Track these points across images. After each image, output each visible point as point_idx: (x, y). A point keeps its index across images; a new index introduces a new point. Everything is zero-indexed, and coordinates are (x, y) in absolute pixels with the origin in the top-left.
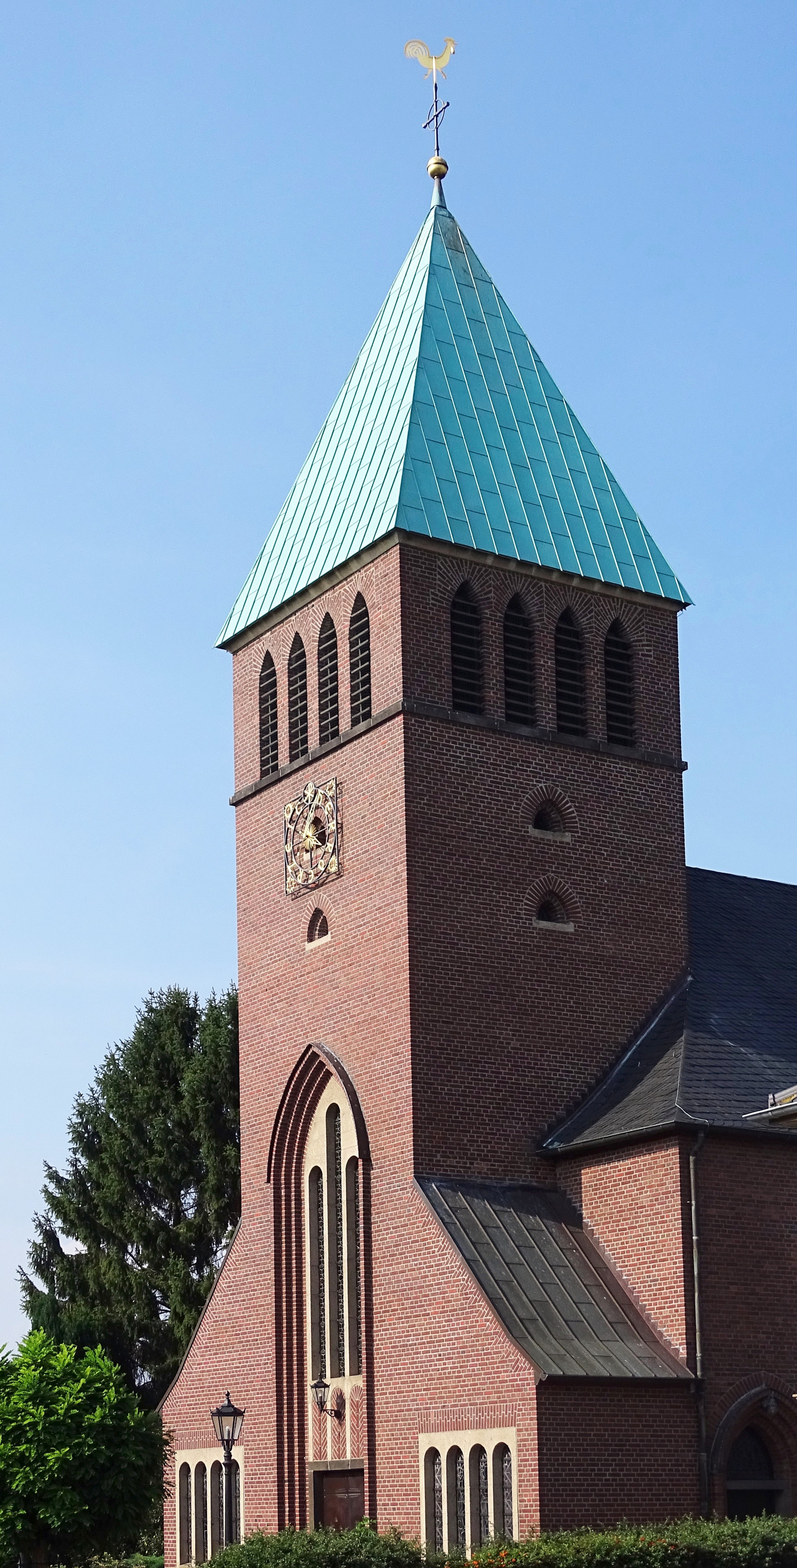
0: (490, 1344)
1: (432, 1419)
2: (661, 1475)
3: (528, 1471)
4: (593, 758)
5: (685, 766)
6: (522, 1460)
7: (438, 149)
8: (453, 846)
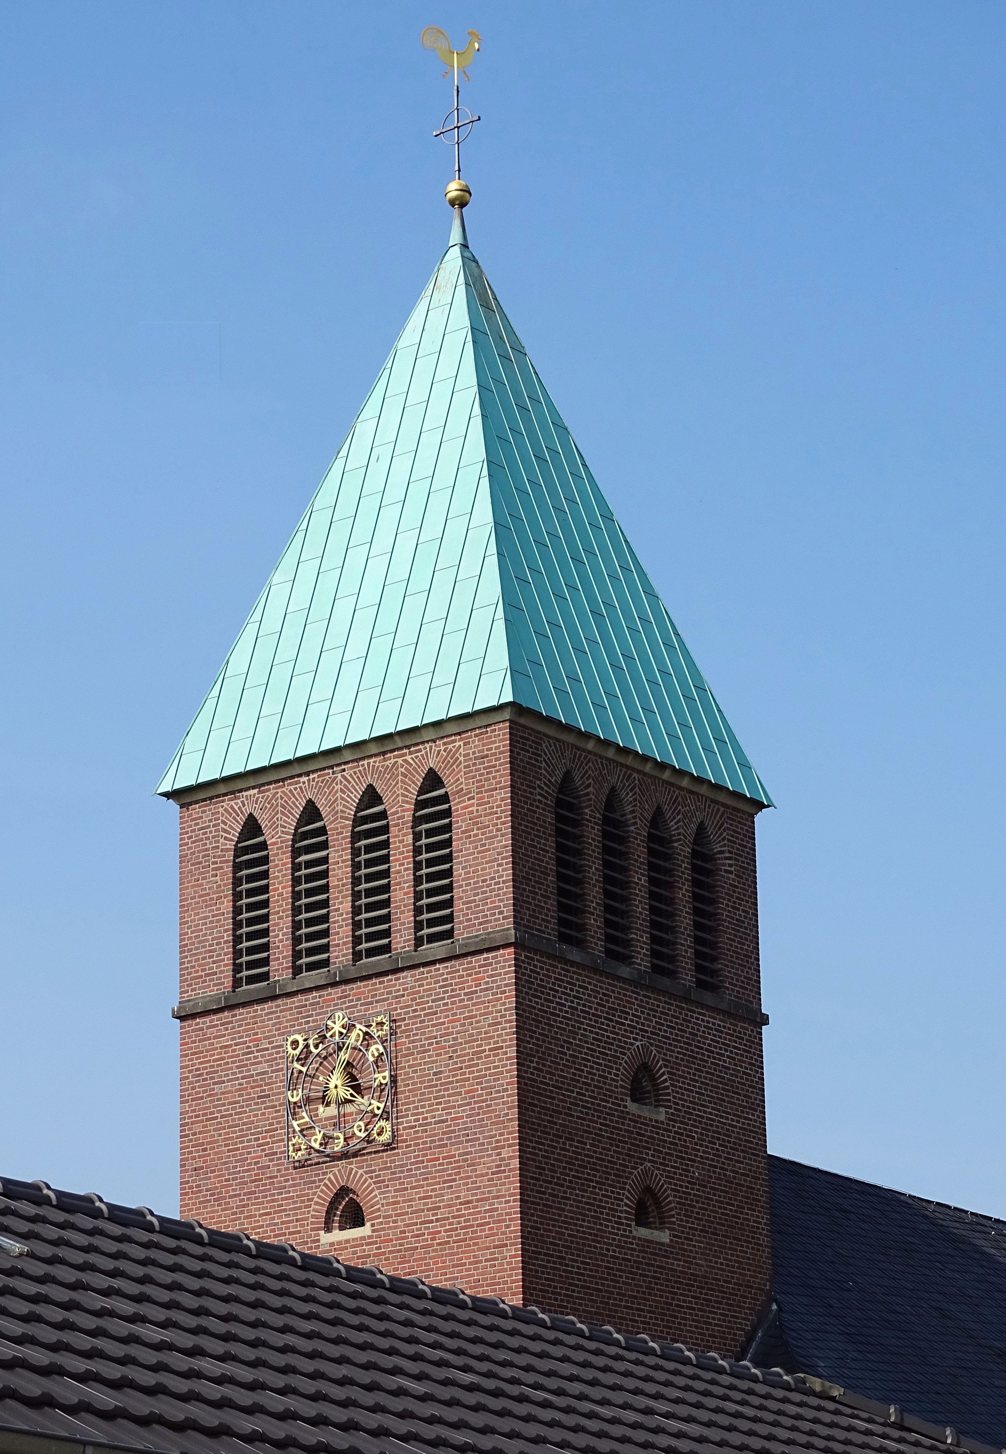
5: (765, 1020)
7: (459, 170)
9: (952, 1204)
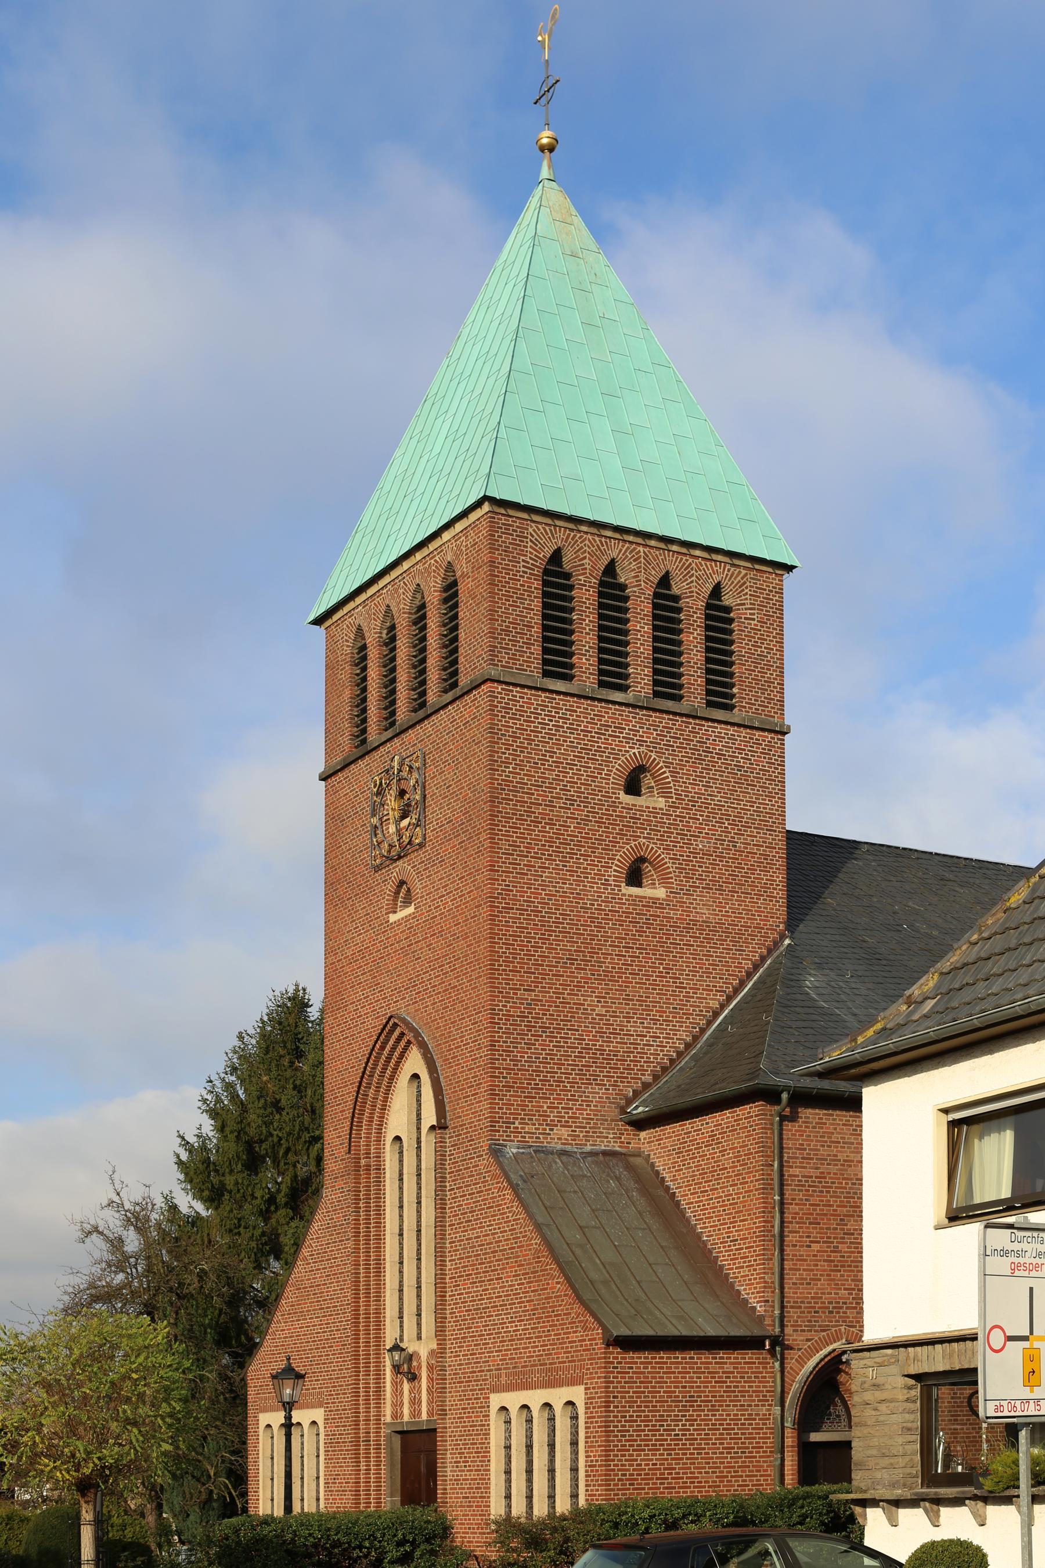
0: (560, 1306)
1: (503, 1380)
2: (733, 1429)
3: (594, 1427)
4: (690, 723)
6: (589, 1418)
8: (539, 813)
9: (934, 851)
